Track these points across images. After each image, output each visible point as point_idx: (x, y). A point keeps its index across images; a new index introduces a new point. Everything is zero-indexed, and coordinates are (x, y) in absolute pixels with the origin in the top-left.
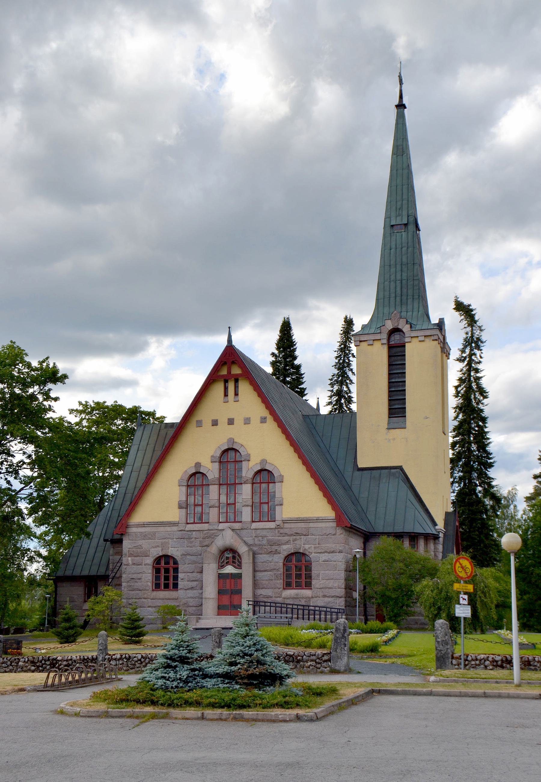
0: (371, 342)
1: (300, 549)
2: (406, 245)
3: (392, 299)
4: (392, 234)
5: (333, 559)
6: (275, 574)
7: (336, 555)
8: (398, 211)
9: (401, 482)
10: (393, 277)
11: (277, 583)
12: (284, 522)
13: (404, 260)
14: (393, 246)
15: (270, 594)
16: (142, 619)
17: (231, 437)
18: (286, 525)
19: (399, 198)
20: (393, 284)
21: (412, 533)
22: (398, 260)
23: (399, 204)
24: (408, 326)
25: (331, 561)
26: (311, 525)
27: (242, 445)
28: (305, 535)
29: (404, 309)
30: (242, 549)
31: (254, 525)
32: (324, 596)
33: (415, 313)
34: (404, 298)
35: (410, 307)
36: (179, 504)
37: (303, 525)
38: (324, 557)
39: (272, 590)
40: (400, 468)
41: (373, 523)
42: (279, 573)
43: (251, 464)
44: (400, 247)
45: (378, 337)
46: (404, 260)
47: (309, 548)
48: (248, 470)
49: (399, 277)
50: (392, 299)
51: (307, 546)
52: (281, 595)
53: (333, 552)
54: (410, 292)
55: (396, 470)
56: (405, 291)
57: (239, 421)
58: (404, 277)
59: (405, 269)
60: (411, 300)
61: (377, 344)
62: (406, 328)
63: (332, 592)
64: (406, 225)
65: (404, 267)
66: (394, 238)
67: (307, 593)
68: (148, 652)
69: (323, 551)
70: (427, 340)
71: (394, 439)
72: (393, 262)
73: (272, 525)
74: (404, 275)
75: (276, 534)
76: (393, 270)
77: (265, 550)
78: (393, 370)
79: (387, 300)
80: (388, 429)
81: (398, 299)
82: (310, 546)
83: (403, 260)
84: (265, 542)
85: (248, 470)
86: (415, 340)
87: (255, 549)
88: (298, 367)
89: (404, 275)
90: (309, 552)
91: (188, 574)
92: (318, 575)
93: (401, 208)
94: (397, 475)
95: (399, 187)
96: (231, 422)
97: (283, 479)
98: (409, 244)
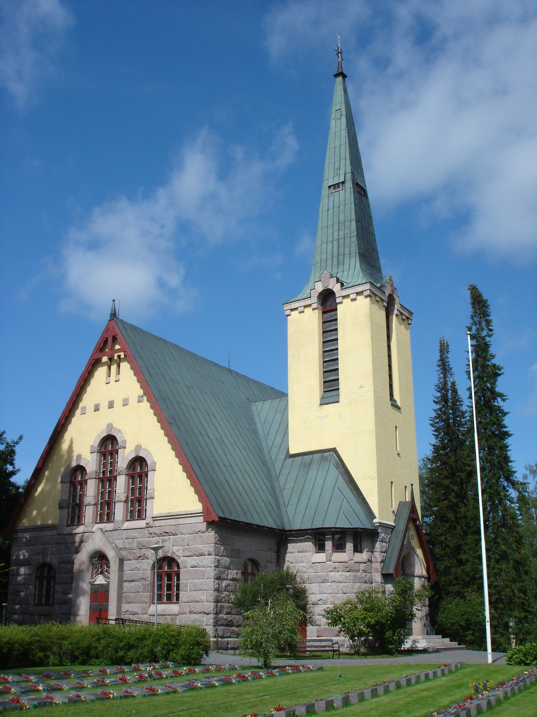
0: (301, 309)
1: (168, 552)
2: (344, 203)
3: (329, 261)
4: (330, 195)
5: (201, 564)
6: (143, 584)
7: (204, 559)
8: (336, 171)
9: (332, 467)
10: (330, 238)
11: (144, 596)
12: (155, 519)
13: (342, 218)
14: (331, 207)
15: (136, 610)
16: (207, 655)
17: (110, 422)
18: (157, 523)
19: (337, 158)
20: (330, 245)
21: (333, 528)
22: (336, 220)
23: (337, 164)
24: (339, 284)
25: (200, 567)
26: (181, 521)
27: (119, 430)
28: (174, 535)
29: (341, 269)
30: (111, 554)
31: (127, 525)
32: (191, 612)
33: (351, 272)
34: (341, 258)
35: (346, 267)
36: (59, 503)
37: (172, 522)
38: (194, 561)
39: (140, 604)
40: (334, 450)
41: (291, 519)
42: (147, 583)
43: (127, 451)
44: (338, 206)
45: (308, 302)
46: (342, 218)
47: (178, 550)
48: (124, 458)
49: (336, 237)
50: (329, 261)
51: (175, 549)
52: (148, 611)
53: (202, 555)
54: (347, 251)
55: (329, 453)
56: (341, 250)
57: (118, 404)
58: (341, 236)
59: (342, 227)
60: (348, 258)
61: (308, 310)
62: (336, 288)
63: (198, 607)
64: (343, 183)
65: (340, 225)
66: (331, 198)
67: (174, 608)
68: (191, 694)
69: (191, 554)
70: (359, 298)
71: (327, 416)
72: (330, 223)
73: (142, 524)
74: (341, 233)
75: (145, 535)
76: (330, 231)
77: (134, 555)
78: (327, 337)
79: (324, 263)
80: (321, 404)
81: (335, 260)
82: (178, 548)
83: (340, 219)
84: (135, 545)
85: (124, 458)
86: (347, 301)
87: (124, 553)
88: (496, 381)
89: (341, 233)
90: (177, 556)
91: (63, 586)
92: (186, 586)
93: (339, 168)
94: (329, 459)
95: (337, 149)
96: (111, 405)
97: (155, 467)
98: (346, 202)
